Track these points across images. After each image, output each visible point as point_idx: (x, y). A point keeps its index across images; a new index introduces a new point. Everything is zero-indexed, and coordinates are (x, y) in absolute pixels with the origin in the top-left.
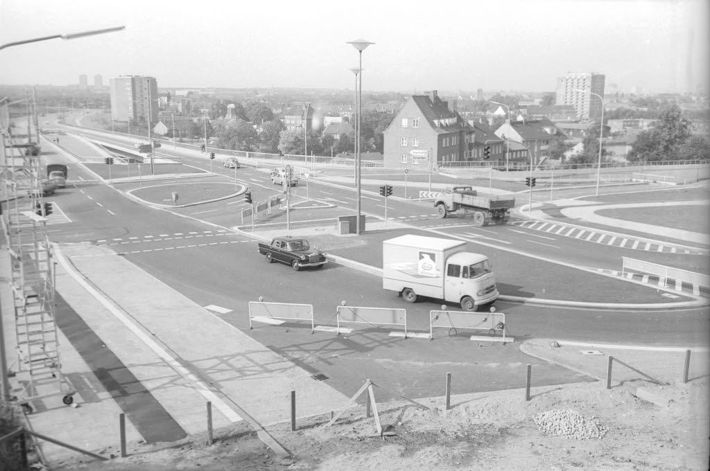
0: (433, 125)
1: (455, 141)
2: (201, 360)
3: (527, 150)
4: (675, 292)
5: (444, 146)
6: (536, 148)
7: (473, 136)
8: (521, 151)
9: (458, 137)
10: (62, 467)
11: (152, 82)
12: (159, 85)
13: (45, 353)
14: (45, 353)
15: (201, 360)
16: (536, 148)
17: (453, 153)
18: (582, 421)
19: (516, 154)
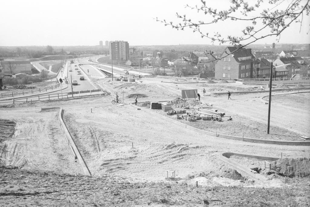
0: (237, 60)
1: (248, 67)
2: (250, 43)
3: (288, 71)
4: (262, 85)
5: (244, 74)
6: (293, 70)
7: (259, 65)
8: (284, 71)
9: (250, 65)
10: (241, 48)
11: (127, 44)
12: (130, 45)
13: (73, 97)
14: (73, 97)
15: (250, 43)
16: (293, 70)
17: (243, 73)
18: (203, 194)
19: (282, 73)
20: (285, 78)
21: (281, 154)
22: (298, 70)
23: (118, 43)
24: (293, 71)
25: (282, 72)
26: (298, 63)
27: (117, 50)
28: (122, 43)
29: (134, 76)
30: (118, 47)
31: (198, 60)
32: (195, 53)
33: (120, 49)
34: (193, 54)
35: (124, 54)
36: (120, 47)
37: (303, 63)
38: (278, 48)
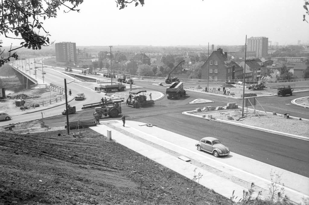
3: (252, 73)
6: (255, 71)
8: (250, 73)
11: (74, 44)
16: (255, 71)
20: (252, 79)
21: (271, 176)
22: (260, 71)
23: (66, 44)
24: (255, 73)
25: (248, 73)
26: (259, 65)
27: (65, 50)
28: (69, 45)
29: (202, 199)
30: (66, 49)
31: (5, 95)
32: (147, 54)
33: (68, 51)
34: (145, 56)
35: (72, 56)
36: (68, 48)
37: (263, 65)
38: (138, 67)
